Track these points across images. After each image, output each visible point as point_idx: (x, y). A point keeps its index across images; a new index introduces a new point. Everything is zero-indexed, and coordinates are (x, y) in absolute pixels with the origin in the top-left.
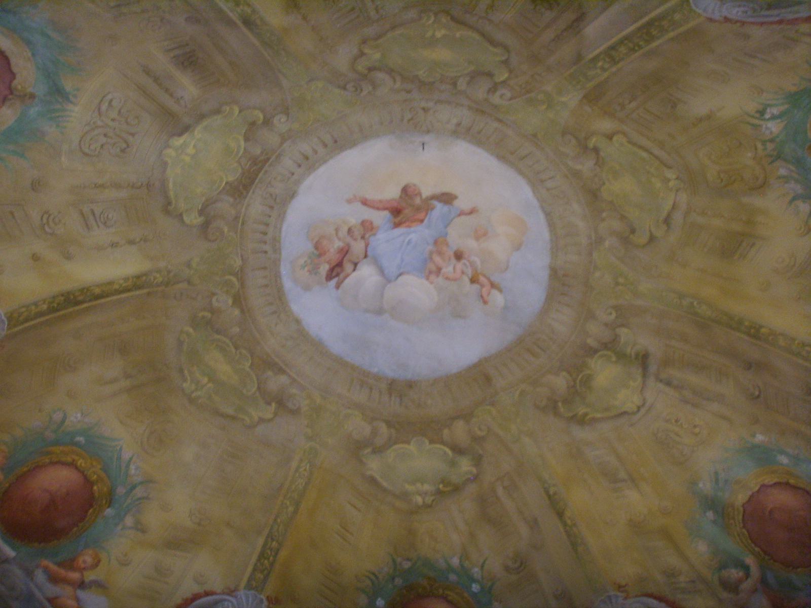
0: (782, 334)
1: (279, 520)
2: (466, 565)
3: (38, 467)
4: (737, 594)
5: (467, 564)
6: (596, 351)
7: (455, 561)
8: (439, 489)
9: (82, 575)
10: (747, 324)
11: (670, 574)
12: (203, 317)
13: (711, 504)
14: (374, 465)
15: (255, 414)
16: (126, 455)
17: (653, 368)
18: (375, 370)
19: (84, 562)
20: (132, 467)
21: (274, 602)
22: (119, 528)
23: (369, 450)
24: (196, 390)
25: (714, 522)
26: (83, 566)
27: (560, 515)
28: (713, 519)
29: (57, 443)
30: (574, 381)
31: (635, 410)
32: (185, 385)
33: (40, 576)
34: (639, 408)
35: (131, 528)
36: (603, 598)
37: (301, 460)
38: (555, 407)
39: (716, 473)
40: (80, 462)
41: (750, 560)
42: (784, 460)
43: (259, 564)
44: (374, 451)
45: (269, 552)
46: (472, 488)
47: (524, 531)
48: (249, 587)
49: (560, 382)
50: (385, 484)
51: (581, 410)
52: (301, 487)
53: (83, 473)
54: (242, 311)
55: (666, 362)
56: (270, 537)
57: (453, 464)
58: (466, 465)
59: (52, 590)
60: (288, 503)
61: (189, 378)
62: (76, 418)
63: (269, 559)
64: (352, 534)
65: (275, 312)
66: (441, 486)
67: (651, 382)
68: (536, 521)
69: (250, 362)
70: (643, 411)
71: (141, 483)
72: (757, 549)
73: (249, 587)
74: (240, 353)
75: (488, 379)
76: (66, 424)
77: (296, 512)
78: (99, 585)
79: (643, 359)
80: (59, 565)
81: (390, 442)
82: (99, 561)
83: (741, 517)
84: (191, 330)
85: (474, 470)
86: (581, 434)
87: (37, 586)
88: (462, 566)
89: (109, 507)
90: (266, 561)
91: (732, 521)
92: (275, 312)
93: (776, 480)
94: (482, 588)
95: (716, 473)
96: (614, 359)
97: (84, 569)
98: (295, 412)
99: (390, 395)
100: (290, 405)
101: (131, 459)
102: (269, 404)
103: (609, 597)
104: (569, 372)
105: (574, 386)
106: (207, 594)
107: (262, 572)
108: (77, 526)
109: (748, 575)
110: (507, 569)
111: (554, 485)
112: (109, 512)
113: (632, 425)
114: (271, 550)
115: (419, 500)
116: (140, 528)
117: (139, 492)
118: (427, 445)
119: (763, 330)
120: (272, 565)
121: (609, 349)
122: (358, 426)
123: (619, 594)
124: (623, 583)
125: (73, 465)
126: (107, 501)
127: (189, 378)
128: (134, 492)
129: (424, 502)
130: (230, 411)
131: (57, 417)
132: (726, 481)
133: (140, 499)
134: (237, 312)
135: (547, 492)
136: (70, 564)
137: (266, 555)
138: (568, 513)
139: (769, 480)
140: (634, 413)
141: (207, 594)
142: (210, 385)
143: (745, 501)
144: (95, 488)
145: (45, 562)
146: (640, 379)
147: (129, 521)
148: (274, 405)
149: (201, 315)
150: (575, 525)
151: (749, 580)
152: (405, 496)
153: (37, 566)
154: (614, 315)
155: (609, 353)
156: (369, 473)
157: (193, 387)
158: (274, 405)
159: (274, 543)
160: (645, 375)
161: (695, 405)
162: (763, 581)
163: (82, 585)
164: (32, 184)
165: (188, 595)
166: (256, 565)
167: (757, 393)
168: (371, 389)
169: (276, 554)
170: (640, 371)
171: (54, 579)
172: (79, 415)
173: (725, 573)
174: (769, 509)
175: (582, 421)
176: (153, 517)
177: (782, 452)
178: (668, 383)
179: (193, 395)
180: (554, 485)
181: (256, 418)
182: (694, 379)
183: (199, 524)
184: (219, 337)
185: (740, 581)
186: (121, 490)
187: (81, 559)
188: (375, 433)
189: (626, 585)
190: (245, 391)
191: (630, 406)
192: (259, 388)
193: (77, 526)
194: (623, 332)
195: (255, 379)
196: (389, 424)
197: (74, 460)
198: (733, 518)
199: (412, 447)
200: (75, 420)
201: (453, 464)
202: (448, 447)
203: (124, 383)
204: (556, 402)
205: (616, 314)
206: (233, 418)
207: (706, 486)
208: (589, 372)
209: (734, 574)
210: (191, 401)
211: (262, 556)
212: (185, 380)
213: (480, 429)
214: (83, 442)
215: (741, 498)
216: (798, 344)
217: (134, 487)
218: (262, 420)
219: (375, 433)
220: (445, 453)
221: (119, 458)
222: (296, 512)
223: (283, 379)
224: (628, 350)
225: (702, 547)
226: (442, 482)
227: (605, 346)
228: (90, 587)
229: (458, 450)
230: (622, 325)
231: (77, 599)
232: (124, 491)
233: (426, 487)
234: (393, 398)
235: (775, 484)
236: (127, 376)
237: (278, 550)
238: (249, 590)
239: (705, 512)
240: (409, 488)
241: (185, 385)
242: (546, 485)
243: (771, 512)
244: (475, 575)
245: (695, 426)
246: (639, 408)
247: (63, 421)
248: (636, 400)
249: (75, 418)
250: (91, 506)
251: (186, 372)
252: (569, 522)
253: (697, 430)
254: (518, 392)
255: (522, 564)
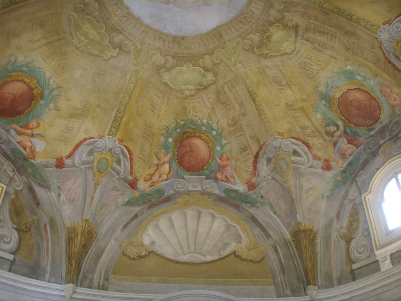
0: (363, 19)
1: (122, 104)
2: (209, 123)
3: (7, 83)
4: (333, 138)
5: (210, 122)
6: (274, 23)
7: (205, 121)
8: (197, 88)
9: (32, 131)
10: (346, 13)
11: (303, 128)
12: (80, 7)
13: (324, 96)
14: (166, 77)
15: (109, 54)
16: (48, 75)
17: (300, 33)
18: (166, 32)
19: (33, 125)
20: (51, 81)
21: (121, 141)
22: (48, 109)
23: (164, 70)
24: (79, 43)
25: (325, 105)
26: (32, 127)
27: (254, 100)
28: (324, 104)
29: (13, 71)
30: (263, 37)
31: (291, 52)
32: (73, 41)
33: (13, 132)
34: (293, 51)
35: (53, 109)
36: (272, 138)
37: (131, 75)
38: (253, 50)
39: (327, 83)
40: (26, 79)
41: (340, 123)
42: (359, 78)
43: (113, 124)
44: (166, 71)
45: (118, 118)
46: (213, 87)
47: (237, 107)
48: (109, 135)
49: (256, 38)
50: (171, 86)
51: (266, 52)
52: (132, 88)
53: (28, 84)
54: (100, 4)
55: (307, 30)
56: (118, 111)
57: (204, 76)
58: (210, 77)
59: (19, 138)
60: (126, 95)
61: (75, 37)
62: (22, 59)
63: (118, 122)
64: (156, 109)
65: (116, 4)
66: (198, 86)
67: (299, 39)
68: (242, 103)
69: (105, 29)
70: (295, 53)
71: (56, 88)
72: (343, 118)
73: (109, 135)
74: (100, 25)
75: (221, 36)
76: (17, 62)
77: (129, 100)
78: (41, 136)
79: (296, 28)
80: (21, 127)
81: (174, 67)
82: (39, 124)
83: (337, 103)
84: (74, 14)
85: (214, 79)
86: (264, 62)
87: (12, 137)
88: (208, 123)
89: (41, 100)
90: (117, 123)
91: (333, 105)
92: (116, 4)
93: (355, 87)
94: (217, 133)
95: (327, 83)
96: (282, 28)
97: (33, 128)
98: (128, 52)
99: (174, 43)
100: (125, 49)
101: (50, 77)
102: (115, 49)
103: (275, 138)
104: (260, 33)
105: (262, 40)
106: (90, 138)
107: (115, 127)
108: (28, 109)
109: (338, 129)
110: (229, 124)
111: (252, 87)
112: (42, 102)
113: (289, 59)
114: (119, 117)
115: (188, 93)
116: (58, 109)
117: (55, 92)
118: (191, 67)
119: (354, 17)
120: (119, 124)
121: (280, 23)
122: (158, 59)
123: (279, 137)
124: (281, 132)
125: (22, 81)
126: (40, 98)
127: (75, 37)
128: (53, 93)
129: (190, 94)
130: (96, 53)
131: (13, 59)
132: (332, 87)
133: (56, 95)
134: (97, 4)
135: (248, 89)
136: (26, 126)
137: (116, 120)
138: (257, 100)
139: (351, 87)
140: (290, 54)
141: (90, 138)
142: (86, 41)
143: (339, 96)
144: (34, 91)
145: (15, 126)
146: (294, 38)
147: (52, 106)
148: (117, 49)
149: (79, 6)
150: (261, 105)
151: (339, 131)
152: (181, 91)
153: (11, 128)
154: (283, 6)
155: (280, 24)
156: (164, 81)
157: (78, 42)
158: (117, 49)
159: (120, 114)
160: (296, 36)
161: (319, 51)
162: (345, 132)
163: (32, 136)
164: (84, 132)
165: (82, 139)
166: (112, 124)
167: (349, 47)
168: (164, 40)
169: (121, 119)
170: (294, 33)
171: (19, 133)
172: (23, 58)
173: (328, 128)
174: (350, 100)
175: (266, 57)
176: (63, 104)
177: (359, 74)
178: (307, 40)
179: (78, 45)
180: (252, 87)
181: (109, 56)
182: (320, 38)
183: (85, 107)
184: (89, 17)
185: (335, 132)
186: (46, 92)
187: (31, 124)
188: (166, 61)
189: (283, 133)
190: (103, 43)
191: (288, 51)
192: (110, 41)
193: (28, 109)
194: (287, 14)
195: (108, 37)
196: (173, 57)
197: (23, 79)
198: (334, 104)
199: (185, 68)
200: (21, 60)
201: (204, 76)
202: (201, 68)
203: (44, 41)
204: (253, 47)
205: (284, 5)
206: (99, 56)
207: (322, 89)
208: (270, 33)
209: (332, 128)
210: (77, 48)
211: (115, 120)
212: (74, 39)
213: (218, 60)
214: (27, 70)
215: (338, 95)
216: (370, 24)
217: (52, 91)
218: (112, 57)
219: (166, 61)
220: (200, 70)
221: (44, 77)
222: (129, 100)
223: (121, 36)
224: (289, 24)
225: (319, 116)
226: (199, 85)
227: (278, 21)
228: (36, 136)
229: (206, 70)
230: (287, 11)
231: (31, 142)
232: (48, 92)
233: (191, 87)
234: (175, 45)
235: (354, 89)
236: (45, 38)
237: (122, 117)
238: (109, 136)
239: (321, 100)
240: (183, 87)
241: (73, 41)
242: (247, 87)
243: (351, 102)
244: (214, 127)
245: (319, 61)
246: (293, 51)
247: (16, 61)
248: (292, 47)
249: (21, 59)
250: (33, 100)
251: (74, 35)
252: (258, 104)
253: (319, 63)
254: (235, 42)
255: (236, 122)
